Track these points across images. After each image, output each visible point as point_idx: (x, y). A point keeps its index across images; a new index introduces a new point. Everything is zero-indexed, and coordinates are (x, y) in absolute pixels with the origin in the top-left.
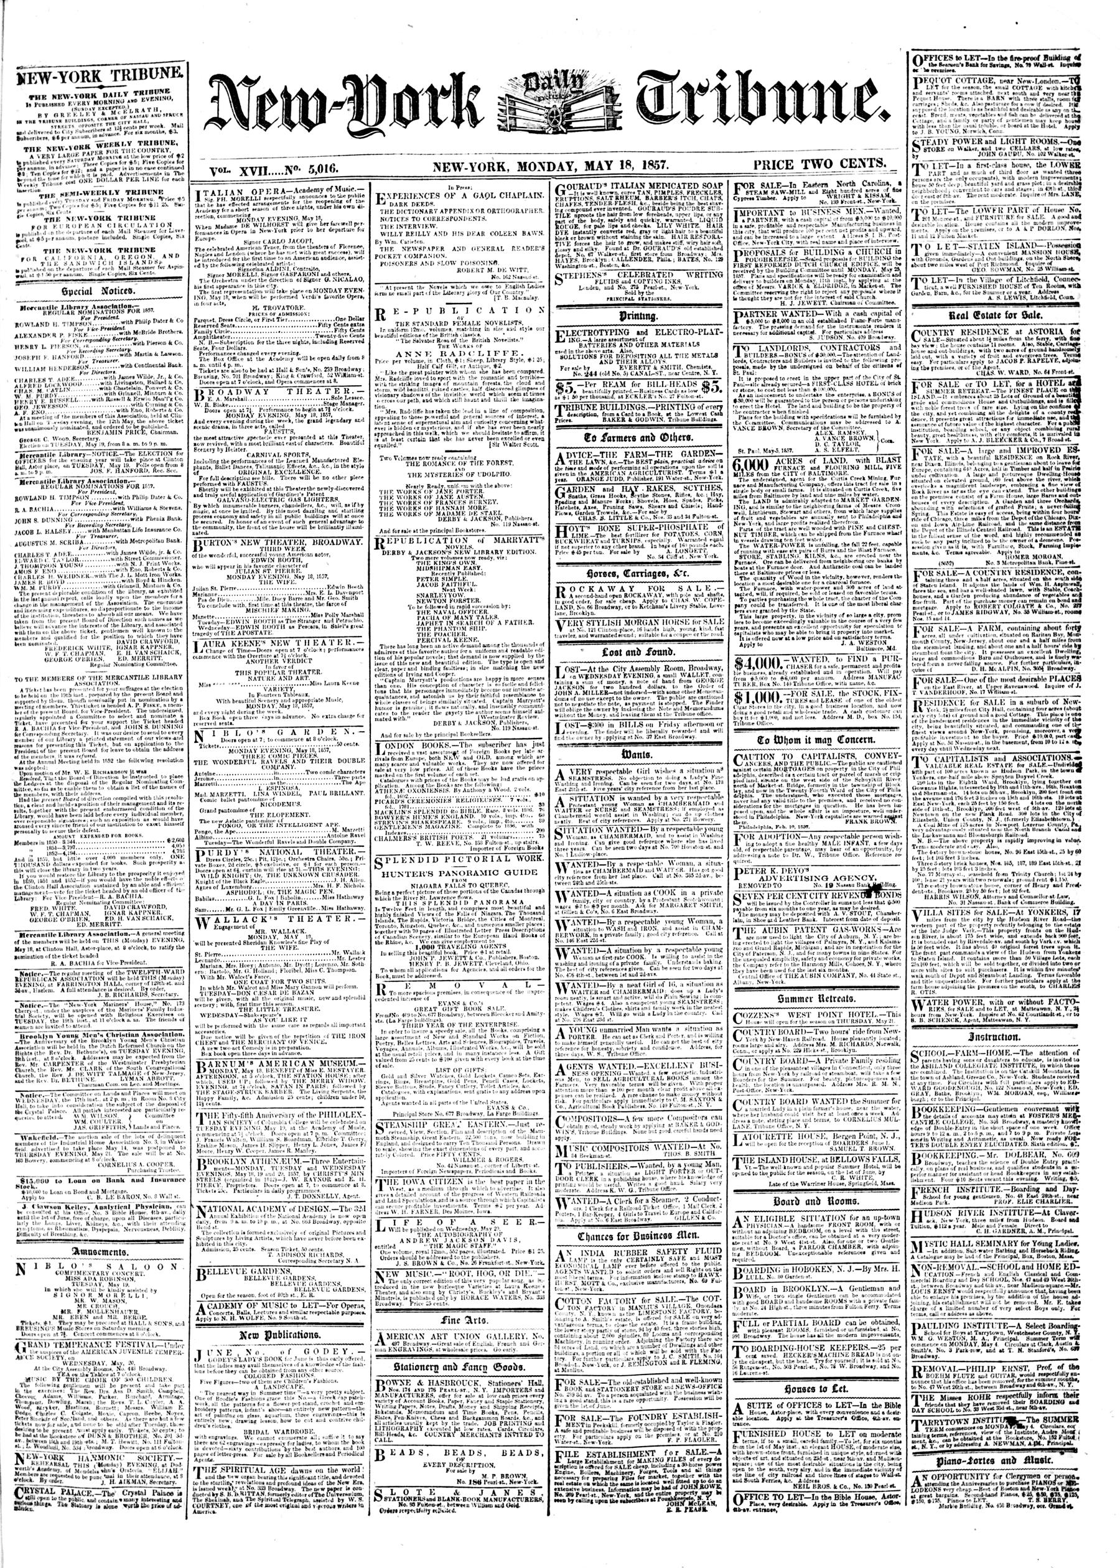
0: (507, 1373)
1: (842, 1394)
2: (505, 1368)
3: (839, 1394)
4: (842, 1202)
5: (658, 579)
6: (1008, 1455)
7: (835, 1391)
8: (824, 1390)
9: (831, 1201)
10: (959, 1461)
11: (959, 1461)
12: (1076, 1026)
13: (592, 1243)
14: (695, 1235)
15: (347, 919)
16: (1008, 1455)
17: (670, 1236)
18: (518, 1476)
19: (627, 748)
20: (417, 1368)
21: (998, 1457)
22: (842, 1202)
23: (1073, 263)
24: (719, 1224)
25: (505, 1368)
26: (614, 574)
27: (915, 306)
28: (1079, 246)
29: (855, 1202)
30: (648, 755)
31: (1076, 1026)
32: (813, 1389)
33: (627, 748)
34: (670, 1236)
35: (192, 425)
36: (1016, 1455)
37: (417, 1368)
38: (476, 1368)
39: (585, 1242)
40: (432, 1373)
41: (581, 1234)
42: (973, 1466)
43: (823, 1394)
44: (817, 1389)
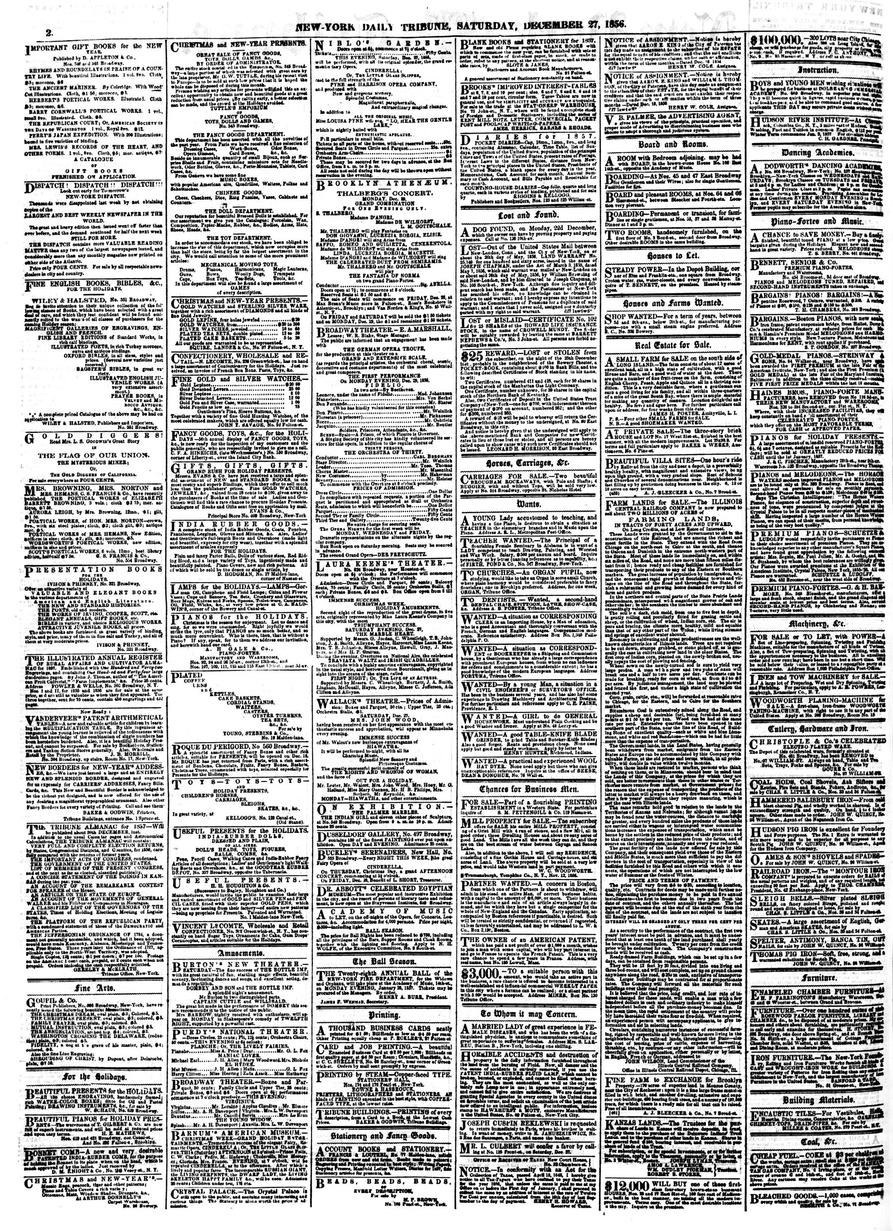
0: (422, 1140)
1: (695, 260)
2: (421, 1136)
3: (691, 260)
4: (694, 145)
5: (545, 467)
6: (829, 217)
7: (688, 257)
8: (680, 256)
9: (685, 144)
10: (790, 222)
11: (790, 222)
12: (883, 615)
13: (491, 794)
14: (575, 789)
15: (295, 880)
16: (829, 217)
17: (555, 790)
18: (430, 1200)
19: (521, 499)
20: (349, 1137)
21: (822, 218)
22: (694, 145)
23: (874, 456)
24: (595, 453)
25: (421, 1136)
26: (509, 464)
27: (753, 1134)
28: (880, 86)
29: (704, 145)
30: (538, 504)
31: (883, 615)
32: (670, 256)
33: (521, 499)
34: (555, 790)
35: (169, 187)
36: (835, 216)
37: (349, 1137)
38: (398, 1136)
39: (486, 794)
40: (361, 1141)
41: (482, 787)
42: (801, 226)
43: (679, 260)
44: (674, 256)
